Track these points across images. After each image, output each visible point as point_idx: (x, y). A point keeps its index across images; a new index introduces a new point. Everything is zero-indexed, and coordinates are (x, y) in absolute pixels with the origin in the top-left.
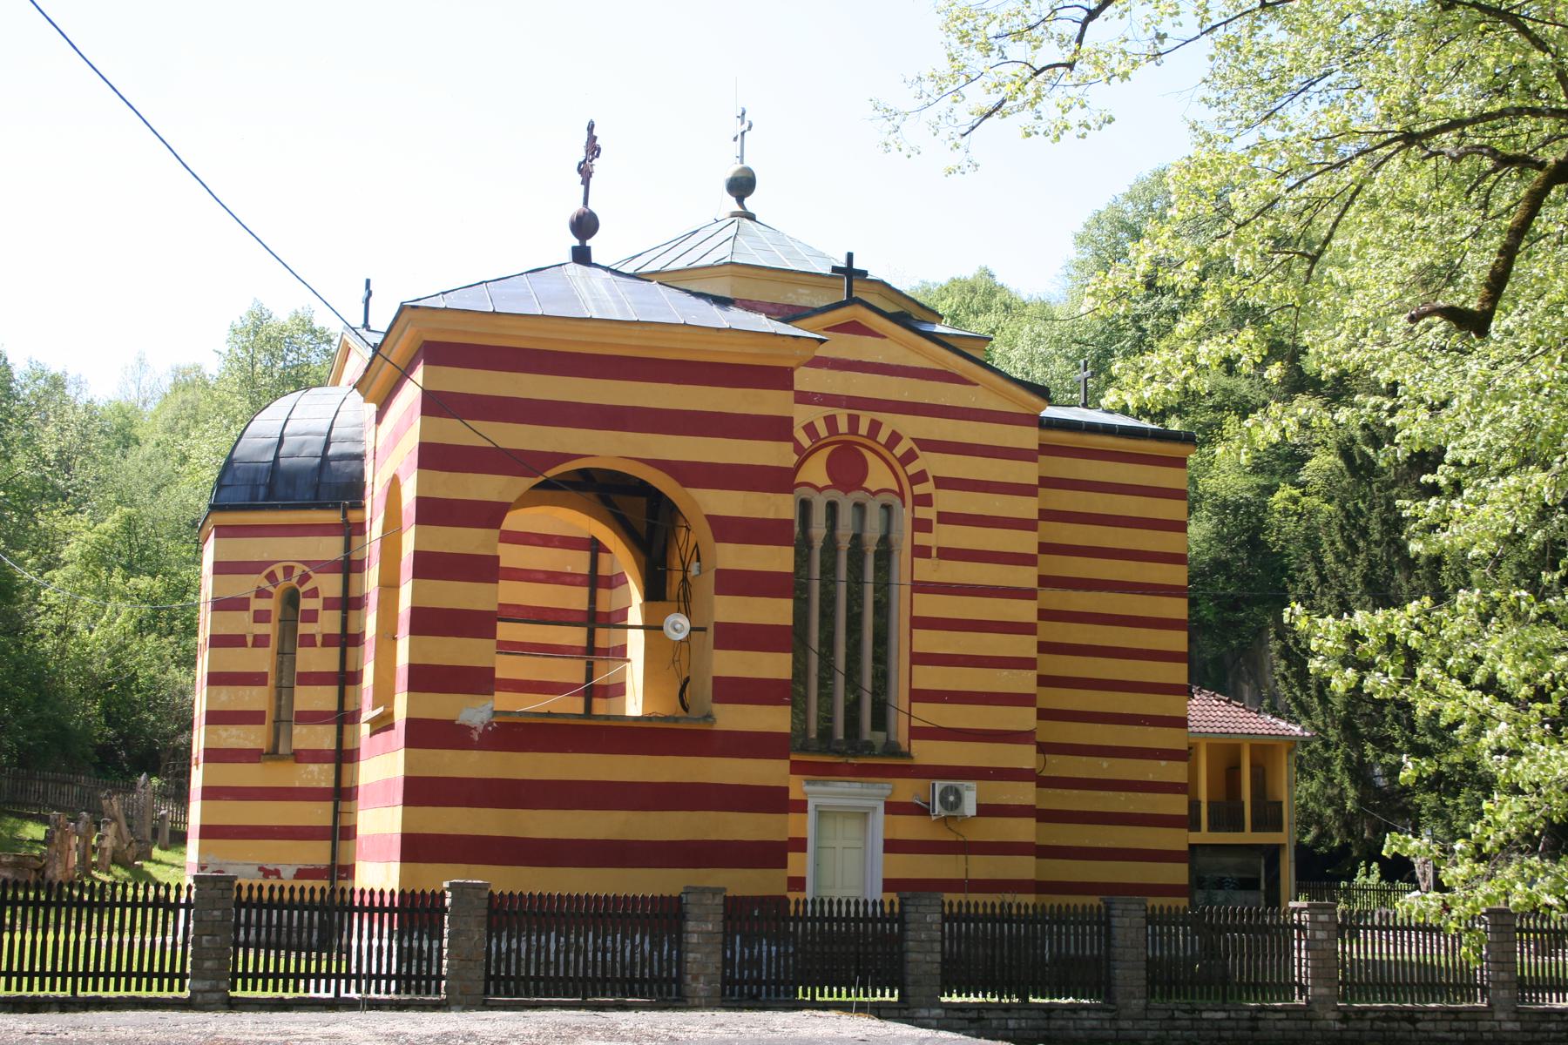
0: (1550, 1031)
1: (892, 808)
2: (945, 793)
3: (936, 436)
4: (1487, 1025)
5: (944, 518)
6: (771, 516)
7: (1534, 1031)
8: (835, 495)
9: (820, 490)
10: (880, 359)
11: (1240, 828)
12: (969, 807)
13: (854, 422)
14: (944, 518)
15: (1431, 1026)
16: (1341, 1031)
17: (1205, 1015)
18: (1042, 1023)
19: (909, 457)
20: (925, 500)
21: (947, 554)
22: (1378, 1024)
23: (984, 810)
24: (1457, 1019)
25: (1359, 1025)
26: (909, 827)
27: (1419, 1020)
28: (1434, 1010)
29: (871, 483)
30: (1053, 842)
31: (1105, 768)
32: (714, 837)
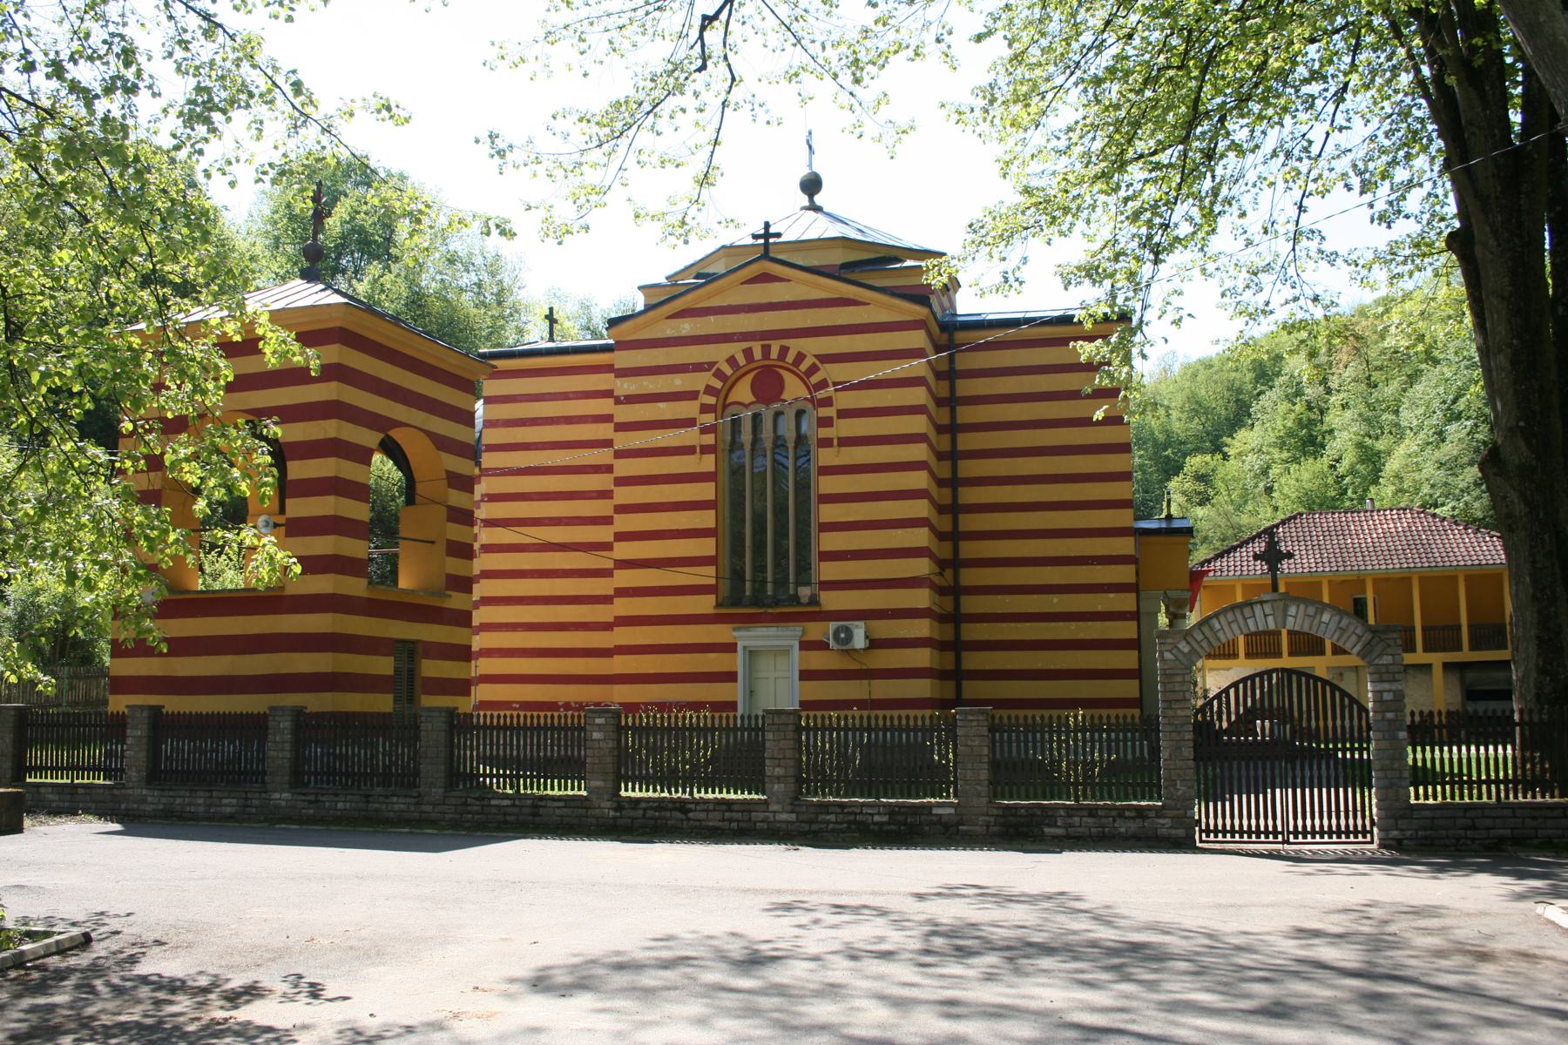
0: (828, 822)
1: (806, 646)
2: (836, 633)
4: (761, 816)
5: (843, 414)
6: (321, 437)
7: (810, 822)
9: (746, 406)
10: (787, 298)
11: (1459, 648)
12: (859, 641)
13: (766, 350)
14: (843, 414)
15: (703, 815)
16: (615, 818)
17: (493, 802)
18: (362, 806)
19: (813, 369)
20: (827, 402)
21: (846, 442)
22: (650, 813)
23: (874, 644)
24: (730, 810)
25: (632, 813)
26: (818, 661)
27: (690, 810)
28: (707, 801)
30: (1009, 667)
31: (1055, 603)
32: (284, 671)
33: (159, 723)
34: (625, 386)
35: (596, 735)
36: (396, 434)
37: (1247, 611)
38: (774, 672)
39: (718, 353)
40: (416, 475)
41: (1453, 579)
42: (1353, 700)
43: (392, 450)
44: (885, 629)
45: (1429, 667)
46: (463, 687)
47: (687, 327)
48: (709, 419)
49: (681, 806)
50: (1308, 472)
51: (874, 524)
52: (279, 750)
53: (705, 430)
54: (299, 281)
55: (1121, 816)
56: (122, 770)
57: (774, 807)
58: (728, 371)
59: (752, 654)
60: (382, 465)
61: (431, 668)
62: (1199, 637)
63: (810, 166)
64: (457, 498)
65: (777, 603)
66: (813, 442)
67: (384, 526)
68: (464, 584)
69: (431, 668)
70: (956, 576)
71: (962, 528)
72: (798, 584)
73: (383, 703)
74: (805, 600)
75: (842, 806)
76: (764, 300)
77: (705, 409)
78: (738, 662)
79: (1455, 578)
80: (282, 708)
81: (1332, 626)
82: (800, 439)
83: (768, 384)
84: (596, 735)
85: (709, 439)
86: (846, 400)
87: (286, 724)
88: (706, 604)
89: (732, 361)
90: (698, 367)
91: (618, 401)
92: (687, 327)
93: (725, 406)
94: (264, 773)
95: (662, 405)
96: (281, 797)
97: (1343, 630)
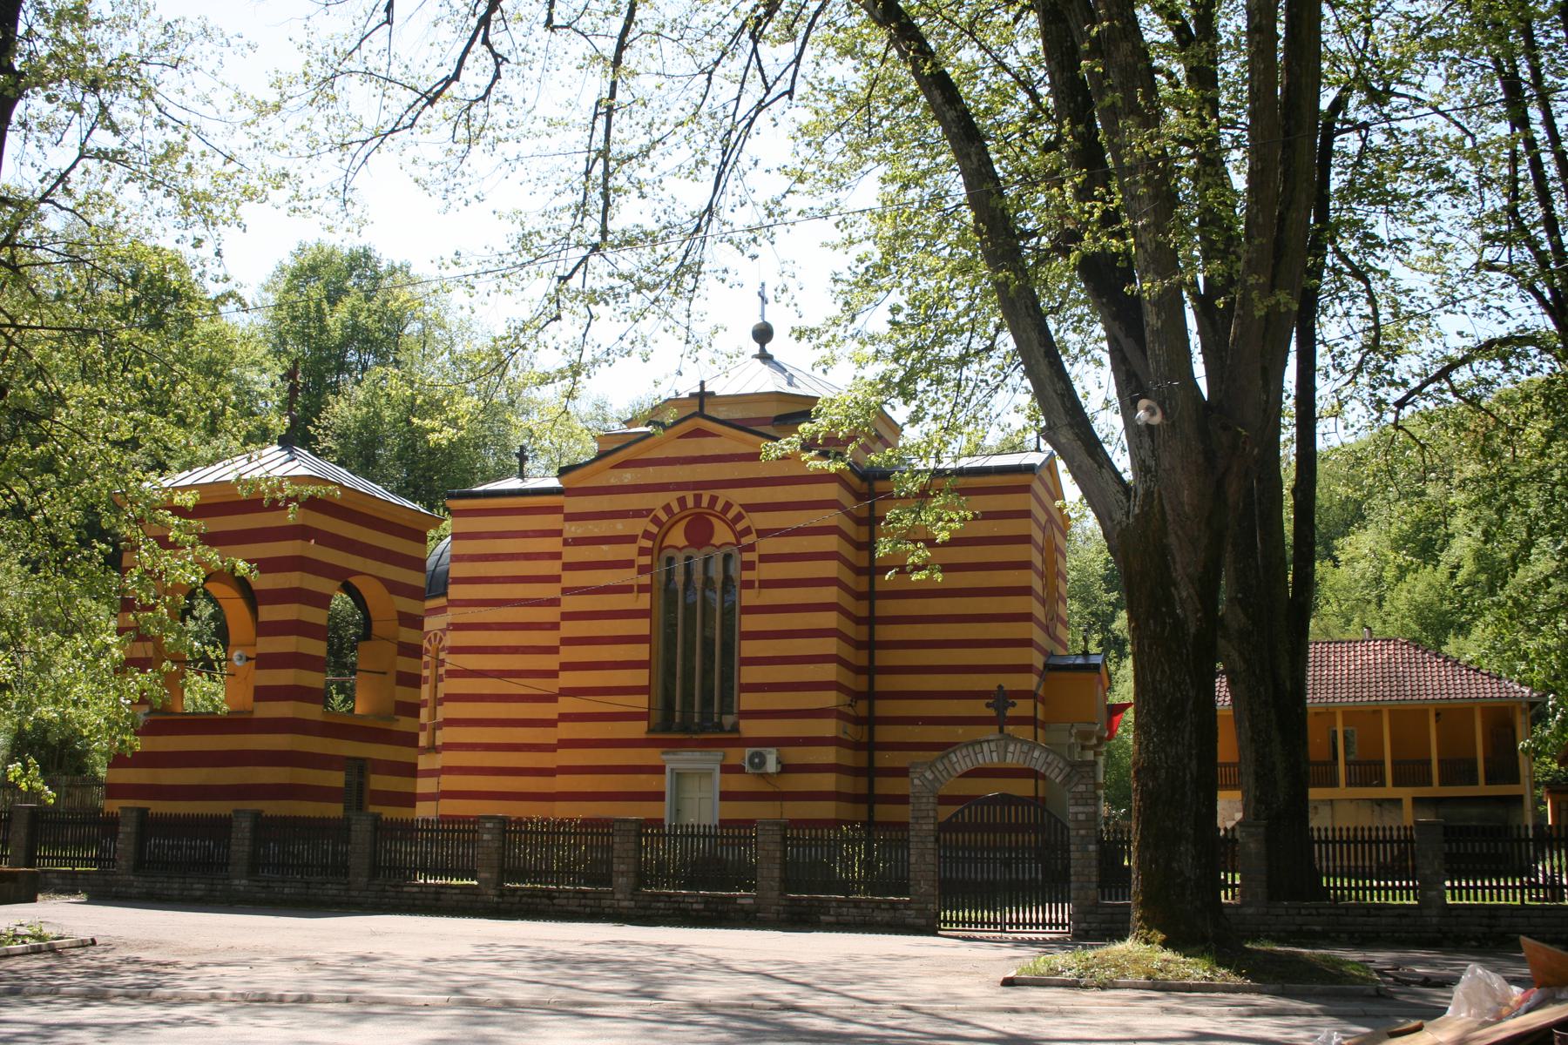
1: (726, 769)
3: (759, 500)
5: (764, 558)
7: (645, 908)
8: (691, 551)
10: (718, 452)
12: (771, 766)
13: (698, 499)
14: (764, 558)
15: (564, 902)
19: (739, 517)
21: (767, 584)
23: (786, 768)
26: (736, 783)
29: (716, 540)
33: (147, 824)
34: (574, 530)
35: (486, 837)
36: (354, 580)
37: (977, 748)
38: (697, 790)
39: (656, 501)
40: (372, 614)
41: (1377, 713)
42: (1057, 820)
43: (348, 588)
44: (796, 755)
45: (1399, 801)
46: (410, 799)
47: (628, 477)
48: (646, 560)
49: (549, 895)
50: (1423, 584)
51: (789, 660)
52: (241, 845)
53: (643, 570)
54: (277, 447)
55: (878, 907)
56: (114, 860)
57: (618, 896)
58: (664, 517)
59: (679, 776)
60: (341, 601)
61: (378, 782)
62: (941, 767)
63: (763, 315)
64: (408, 635)
65: (703, 731)
66: (737, 584)
67: (338, 659)
68: (412, 710)
69: (378, 782)
70: (871, 708)
71: (877, 663)
72: (722, 713)
73: (335, 810)
74: (728, 728)
75: (669, 895)
76: (697, 453)
77: (643, 551)
78: (666, 783)
79: (1426, 712)
80: (244, 811)
81: (1041, 761)
82: (727, 579)
83: (699, 531)
84: (486, 837)
85: (645, 579)
86: (768, 546)
87: (246, 824)
88: (638, 729)
89: (667, 508)
90: (638, 514)
91: (566, 543)
92: (628, 477)
93: (661, 549)
94: (227, 864)
95: (604, 547)
96: (240, 883)
97: (1049, 764)
